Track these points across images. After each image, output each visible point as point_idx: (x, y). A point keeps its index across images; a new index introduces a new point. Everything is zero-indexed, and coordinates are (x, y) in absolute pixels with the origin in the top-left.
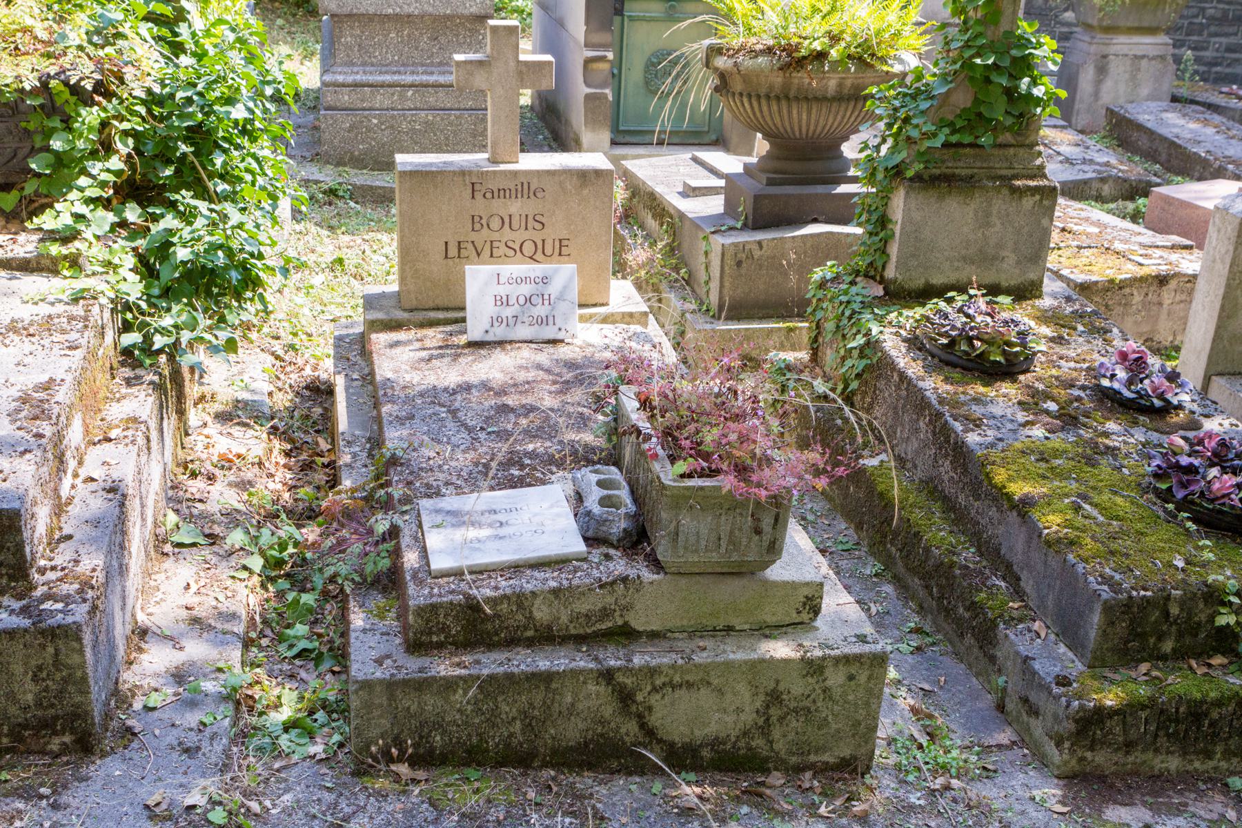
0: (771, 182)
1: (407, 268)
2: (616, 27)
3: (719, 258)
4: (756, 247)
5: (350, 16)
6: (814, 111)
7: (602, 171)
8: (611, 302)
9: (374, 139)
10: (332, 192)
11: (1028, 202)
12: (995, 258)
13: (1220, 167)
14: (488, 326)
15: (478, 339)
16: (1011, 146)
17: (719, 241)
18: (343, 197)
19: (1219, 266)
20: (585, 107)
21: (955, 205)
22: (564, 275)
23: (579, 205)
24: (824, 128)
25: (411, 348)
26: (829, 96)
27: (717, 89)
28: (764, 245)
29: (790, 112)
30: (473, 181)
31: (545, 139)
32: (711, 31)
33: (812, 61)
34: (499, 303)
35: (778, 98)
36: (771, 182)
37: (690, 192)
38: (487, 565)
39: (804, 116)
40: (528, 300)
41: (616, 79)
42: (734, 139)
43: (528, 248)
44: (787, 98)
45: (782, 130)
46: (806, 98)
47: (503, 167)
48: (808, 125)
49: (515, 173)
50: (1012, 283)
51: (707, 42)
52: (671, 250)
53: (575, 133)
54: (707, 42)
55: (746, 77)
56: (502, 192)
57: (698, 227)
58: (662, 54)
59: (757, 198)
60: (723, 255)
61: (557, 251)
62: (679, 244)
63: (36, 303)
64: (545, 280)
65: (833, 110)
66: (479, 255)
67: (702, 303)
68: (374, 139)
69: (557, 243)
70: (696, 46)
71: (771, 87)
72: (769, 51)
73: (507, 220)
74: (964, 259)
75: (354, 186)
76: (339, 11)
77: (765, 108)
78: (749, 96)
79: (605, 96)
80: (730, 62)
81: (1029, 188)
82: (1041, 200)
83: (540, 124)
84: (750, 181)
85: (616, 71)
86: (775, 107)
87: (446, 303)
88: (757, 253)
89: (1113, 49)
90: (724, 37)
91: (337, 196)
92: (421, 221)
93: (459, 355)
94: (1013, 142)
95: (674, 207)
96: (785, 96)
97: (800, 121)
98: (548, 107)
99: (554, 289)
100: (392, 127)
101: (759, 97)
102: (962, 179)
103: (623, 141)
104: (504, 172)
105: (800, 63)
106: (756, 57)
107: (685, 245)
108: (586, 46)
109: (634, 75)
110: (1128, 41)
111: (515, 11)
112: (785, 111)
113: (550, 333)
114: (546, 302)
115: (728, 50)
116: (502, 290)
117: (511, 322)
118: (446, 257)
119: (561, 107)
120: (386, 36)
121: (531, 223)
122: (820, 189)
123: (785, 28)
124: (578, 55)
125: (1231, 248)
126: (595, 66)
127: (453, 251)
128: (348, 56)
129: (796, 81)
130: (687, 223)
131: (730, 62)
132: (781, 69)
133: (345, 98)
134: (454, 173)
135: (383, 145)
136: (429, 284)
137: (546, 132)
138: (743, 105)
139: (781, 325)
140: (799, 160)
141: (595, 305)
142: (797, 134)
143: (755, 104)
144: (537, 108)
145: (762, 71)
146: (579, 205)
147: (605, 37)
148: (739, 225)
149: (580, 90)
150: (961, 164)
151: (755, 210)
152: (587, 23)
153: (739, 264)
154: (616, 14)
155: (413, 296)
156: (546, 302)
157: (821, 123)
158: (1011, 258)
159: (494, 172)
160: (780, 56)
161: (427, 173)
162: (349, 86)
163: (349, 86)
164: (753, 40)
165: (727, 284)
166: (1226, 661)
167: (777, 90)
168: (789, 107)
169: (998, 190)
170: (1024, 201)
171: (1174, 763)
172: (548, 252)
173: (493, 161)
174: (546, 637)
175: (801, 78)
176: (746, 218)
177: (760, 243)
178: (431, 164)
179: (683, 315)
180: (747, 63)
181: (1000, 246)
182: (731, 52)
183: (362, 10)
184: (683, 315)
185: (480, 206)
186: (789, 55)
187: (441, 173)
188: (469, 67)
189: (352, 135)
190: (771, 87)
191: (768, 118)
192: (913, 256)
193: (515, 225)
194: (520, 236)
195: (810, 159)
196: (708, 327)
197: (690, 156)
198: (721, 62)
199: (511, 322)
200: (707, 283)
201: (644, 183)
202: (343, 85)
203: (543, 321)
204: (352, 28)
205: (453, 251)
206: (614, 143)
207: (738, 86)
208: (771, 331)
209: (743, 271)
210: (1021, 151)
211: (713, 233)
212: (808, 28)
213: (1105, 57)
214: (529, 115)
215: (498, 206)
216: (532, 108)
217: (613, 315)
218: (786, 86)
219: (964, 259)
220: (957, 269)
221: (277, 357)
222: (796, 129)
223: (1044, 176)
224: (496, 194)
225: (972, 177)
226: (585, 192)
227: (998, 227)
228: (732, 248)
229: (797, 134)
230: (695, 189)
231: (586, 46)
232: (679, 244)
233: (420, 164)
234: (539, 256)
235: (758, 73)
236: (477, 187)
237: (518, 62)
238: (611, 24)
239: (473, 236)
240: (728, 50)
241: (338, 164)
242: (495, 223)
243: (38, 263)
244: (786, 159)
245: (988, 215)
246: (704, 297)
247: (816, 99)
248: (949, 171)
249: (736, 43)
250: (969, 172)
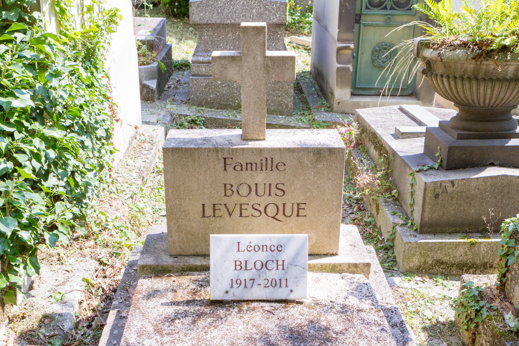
0: (461, 137)
1: (172, 224)
2: (356, 30)
3: (423, 191)
4: (449, 185)
5: (207, 24)
6: (496, 88)
7: (335, 149)
8: (340, 251)
9: (219, 92)
10: (193, 121)
14: (228, 288)
15: (219, 299)
17: (423, 179)
18: (199, 124)
20: (337, 75)
22: (297, 241)
23: (315, 176)
24: (502, 100)
25: (164, 300)
26: (508, 77)
27: (424, 72)
28: (456, 183)
29: (478, 89)
30: (225, 157)
31: (316, 90)
32: (423, 32)
33: (498, 53)
34: (238, 268)
35: (470, 79)
36: (461, 137)
37: (399, 135)
39: (489, 92)
40: (265, 265)
41: (355, 59)
42: (422, 94)
43: (272, 210)
44: (476, 79)
45: (470, 101)
46: (491, 79)
47: (252, 145)
48: (491, 99)
49: (260, 151)
51: (418, 39)
52: (387, 176)
53: (331, 89)
54: (418, 39)
55: (446, 64)
57: (406, 164)
58: (385, 47)
59: (451, 149)
60: (425, 190)
61: (295, 213)
62: (392, 172)
64: (280, 248)
65: (511, 87)
66: (230, 215)
67: (407, 218)
68: (219, 92)
69: (295, 207)
70: (410, 41)
71: (465, 71)
72: (464, 45)
73: (253, 188)
75: (206, 118)
76: (201, 22)
77: (459, 86)
78: (448, 77)
79: (349, 68)
80: (435, 53)
83: (314, 82)
84: (444, 134)
85: (355, 55)
86: (467, 86)
88: (450, 189)
90: (431, 35)
91: (196, 124)
92: (182, 188)
93: (200, 315)
95: (389, 146)
96: (475, 78)
97: (485, 95)
98: (318, 73)
99: (286, 256)
100: (229, 85)
101: (455, 78)
103: (358, 93)
104: (251, 149)
105: (489, 54)
106: (455, 49)
107: (396, 174)
108: (338, 40)
109: (366, 56)
111: (308, 23)
112: (474, 89)
113: (281, 293)
114: (280, 267)
115: (433, 44)
116: (241, 257)
117: (249, 284)
118: (204, 216)
119: (324, 73)
120: (226, 35)
121: (274, 190)
122: (496, 142)
123: (479, 28)
124: (334, 45)
126: (343, 52)
127: (209, 211)
128: (205, 46)
129: (484, 67)
130: (398, 161)
131: (435, 53)
132: (474, 58)
133: (203, 69)
134: (209, 150)
135: (224, 95)
136: (190, 236)
137: (317, 87)
138: (443, 83)
139: (466, 240)
140: (481, 121)
141: (326, 255)
142: (482, 104)
143: (452, 83)
144: (313, 73)
145: (459, 60)
146: (315, 176)
147: (350, 36)
148: (436, 166)
149: (334, 65)
151: (449, 156)
152: (339, 28)
153: (437, 196)
154: (356, 23)
155: (177, 245)
156: (280, 267)
157: (501, 96)
159: (243, 149)
160: (473, 49)
161: (187, 150)
162: (205, 63)
163: (205, 63)
164: (452, 38)
165: (427, 210)
167: (469, 73)
172: (288, 213)
173: (245, 138)
175: (489, 65)
176: (441, 161)
177: (453, 182)
178: (192, 141)
179: (394, 227)
180: (448, 54)
182: (436, 46)
183: (213, 22)
184: (394, 227)
185: (231, 177)
186: (480, 48)
187: (198, 149)
188: (223, 61)
189: (207, 90)
190: (465, 71)
191: (461, 93)
193: (260, 191)
194: (264, 201)
195: (489, 121)
196: (412, 240)
197: (398, 107)
198: (428, 53)
199: (249, 284)
200: (412, 205)
201: (369, 126)
202: (202, 63)
203: (275, 284)
204: (208, 31)
205: (209, 211)
206: (353, 94)
207: (439, 69)
208: (459, 244)
209: (439, 201)
211: (417, 172)
212: (498, 29)
214: (308, 76)
215: (246, 177)
216: (310, 73)
217: (340, 265)
218: (476, 71)
221: (101, 263)
224: (244, 167)
226: (320, 166)
228: (432, 185)
229: (482, 104)
230: (403, 134)
231: (338, 40)
232: (392, 172)
233: (185, 142)
234: (280, 216)
235: (456, 61)
236: (228, 161)
237: (265, 57)
238: (353, 28)
239: (226, 200)
240: (433, 44)
241: (199, 106)
242: (244, 190)
246: (409, 214)
247: (498, 80)
249: (439, 39)
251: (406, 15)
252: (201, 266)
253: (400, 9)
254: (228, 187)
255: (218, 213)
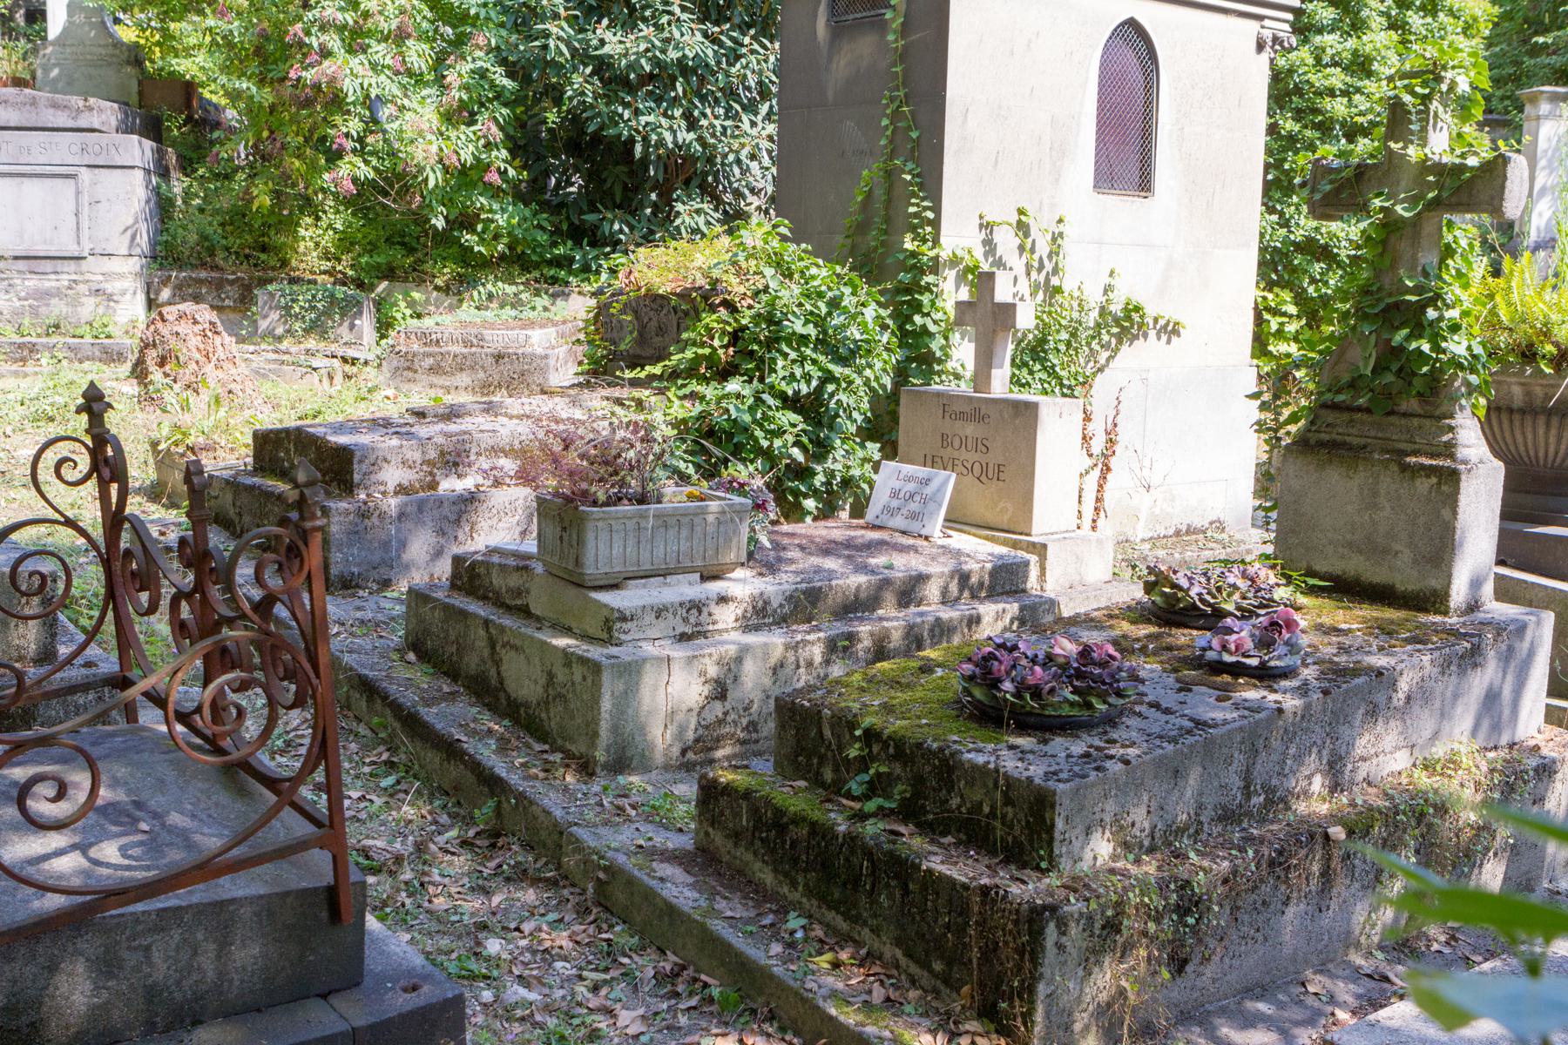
11: (1424, 485)
12: (1385, 551)
16: (1413, 415)
21: (1336, 476)
50: (1410, 588)
64: (927, 482)
74: (1349, 545)
81: (1423, 467)
82: (1439, 483)
94: (1420, 411)
97: (1547, 444)
102: (1350, 448)
150: (1354, 431)
158: (1407, 555)
166: (1052, 925)
168: (1548, 425)
169: (1385, 464)
170: (1418, 482)
171: (767, 877)
192: (1293, 531)
203: (914, 516)
210: (1427, 422)
219: (1349, 545)
220: (1342, 557)
222: (1522, 449)
223: (1452, 456)
225: (1365, 447)
227: (1387, 512)
242: (957, 444)
245: (1375, 494)
248: (1339, 438)
250: (1363, 441)
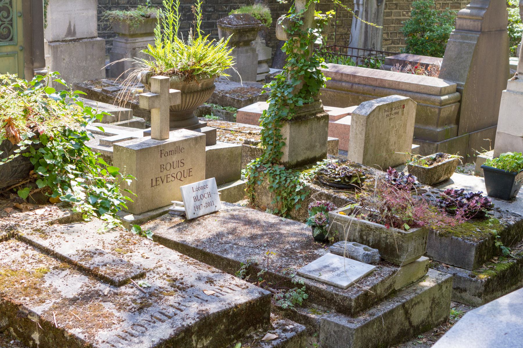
11: (322, 122)
13: (223, 96)
19: (359, 136)
38: (338, 285)
46: (191, 92)
56: (171, 153)
63: (100, 234)
87: (150, 208)
89: (137, 45)
110: (142, 40)
125: (364, 128)
140: (183, 120)
150: (302, 111)
155: (140, 207)
174: (380, 300)
181: (315, 142)
188: (153, 99)
213: (134, 49)
237: (169, 94)
243: (72, 218)
244: (178, 121)
250: (304, 114)
251: (9, 45)
252: (156, 215)
253: (5, 40)
254: (162, 166)
255: (158, 183)
